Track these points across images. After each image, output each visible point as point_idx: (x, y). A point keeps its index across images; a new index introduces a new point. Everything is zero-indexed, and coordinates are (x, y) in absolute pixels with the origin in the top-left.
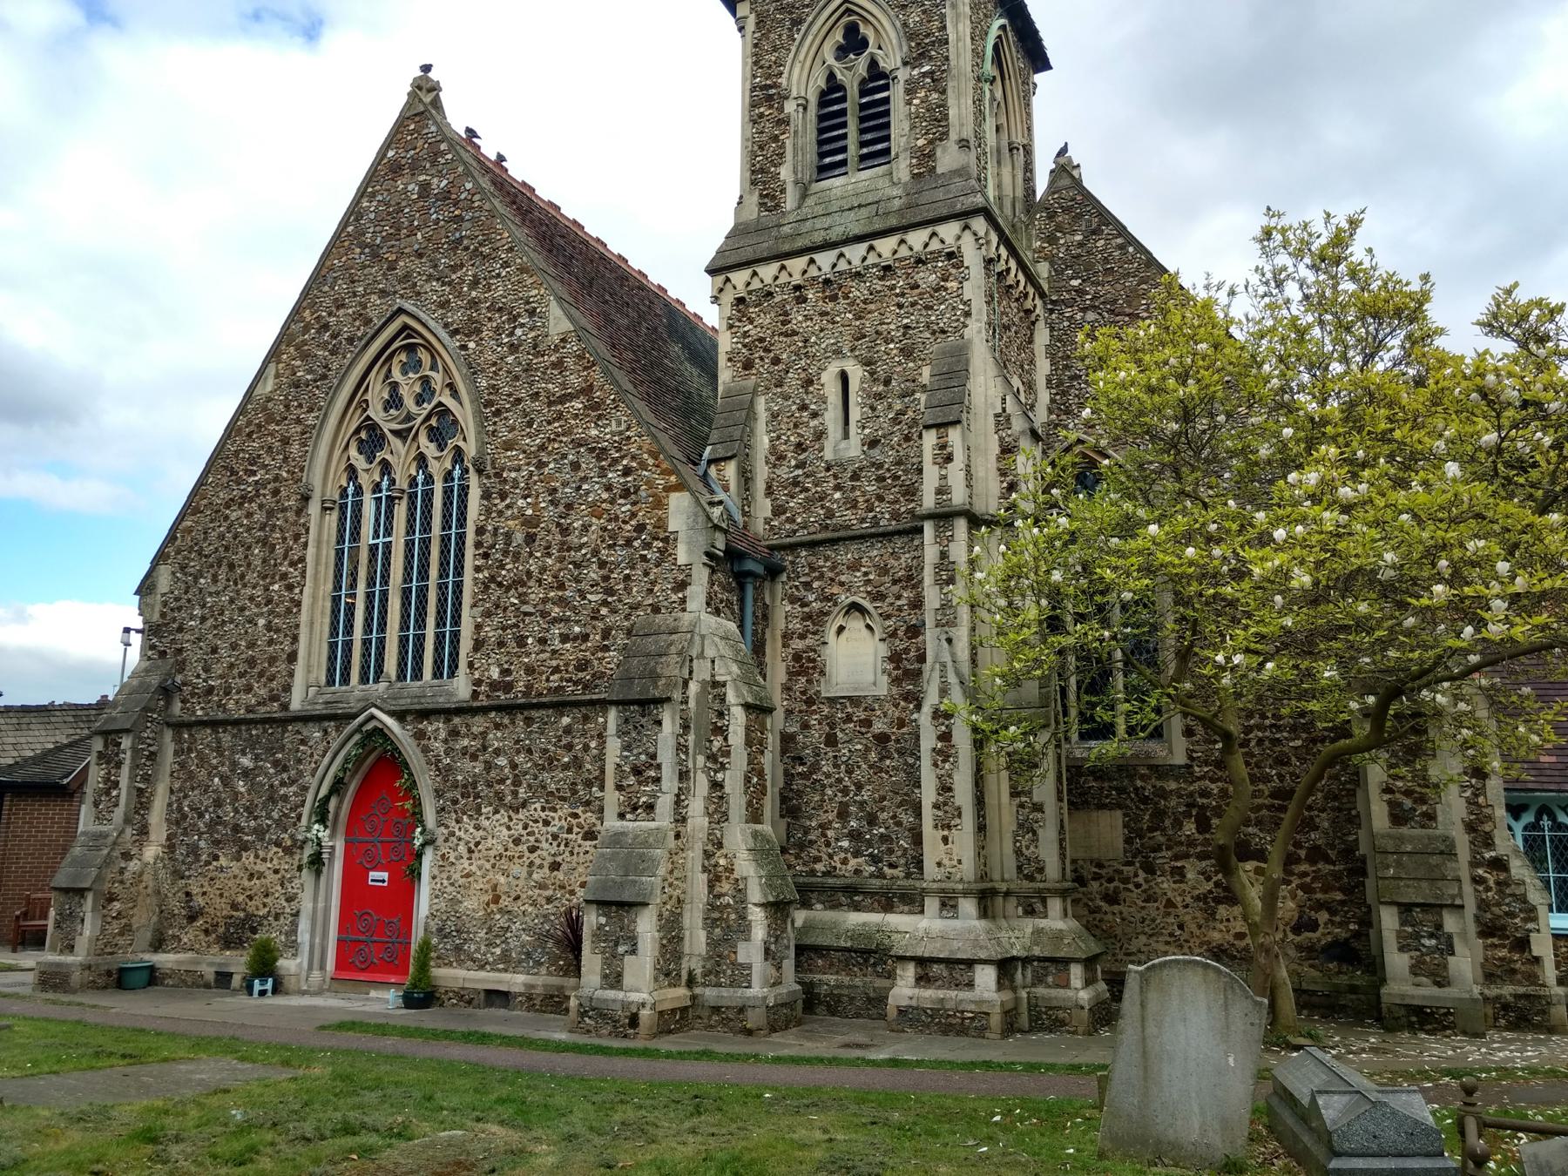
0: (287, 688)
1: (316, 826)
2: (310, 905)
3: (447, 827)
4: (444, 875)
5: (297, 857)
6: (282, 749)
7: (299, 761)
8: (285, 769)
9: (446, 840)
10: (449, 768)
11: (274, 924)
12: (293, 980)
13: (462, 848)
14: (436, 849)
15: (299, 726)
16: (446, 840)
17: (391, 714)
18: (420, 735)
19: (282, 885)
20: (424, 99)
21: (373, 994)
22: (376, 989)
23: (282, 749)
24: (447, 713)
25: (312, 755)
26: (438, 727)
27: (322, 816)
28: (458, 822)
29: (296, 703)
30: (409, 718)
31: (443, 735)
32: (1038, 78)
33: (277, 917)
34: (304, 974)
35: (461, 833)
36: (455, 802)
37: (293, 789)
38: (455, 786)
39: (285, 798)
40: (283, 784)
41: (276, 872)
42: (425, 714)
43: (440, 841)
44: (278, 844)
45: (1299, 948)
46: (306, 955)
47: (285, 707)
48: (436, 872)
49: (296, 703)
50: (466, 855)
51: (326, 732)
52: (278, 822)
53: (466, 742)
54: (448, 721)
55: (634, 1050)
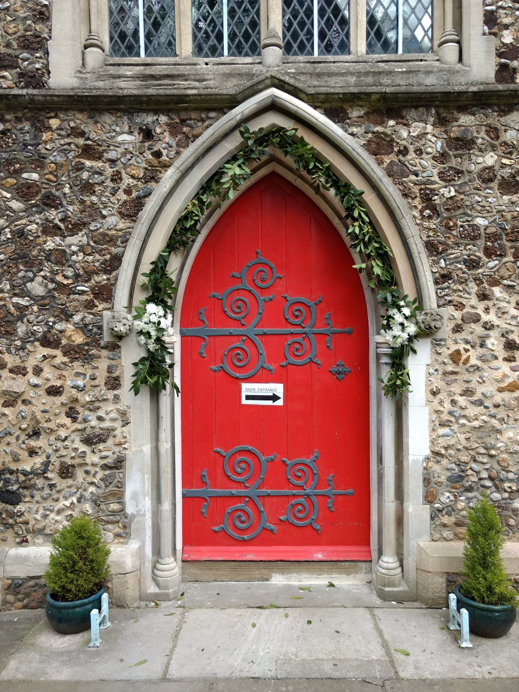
0: (36, 44)
1: (151, 307)
2: (147, 449)
3: (459, 306)
4: (457, 388)
5: (103, 364)
6: (39, 162)
7: (88, 188)
8: (50, 202)
9: (457, 329)
10: (454, 205)
11: (62, 484)
12: (131, 580)
13: (495, 342)
14: (437, 343)
15: (78, 120)
16: (457, 329)
17: (314, 100)
18: (380, 146)
19: (72, 414)
21: (278, 580)
22: (282, 572)
23: (39, 162)
24: (443, 104)
25: (116, 178)
26: (420, 132)
27: (158, 290)
28: (483, 297)
29: (64, 72)
30: (355, 113)
31: (436, 145)
33: (66, 472)
34: (148, 566)
35: (491, 317)
36: (473, 264)
37: (80, 238)
38: (472, 235)
39: (61, 257)
40: (50, 229)
41: (54, 391)
42: (393, 106)
43: (446, 330)
44: (47, 341)
45: (157, 32)
46: (149, 532)
47: (35, 79)
48: (438, 383)
49: (64, 72)
50: (501, 353)
51: (148, 134)
52: (44, 303)
53: (490, 159)
54: (442, 122)
55: (379, 471)
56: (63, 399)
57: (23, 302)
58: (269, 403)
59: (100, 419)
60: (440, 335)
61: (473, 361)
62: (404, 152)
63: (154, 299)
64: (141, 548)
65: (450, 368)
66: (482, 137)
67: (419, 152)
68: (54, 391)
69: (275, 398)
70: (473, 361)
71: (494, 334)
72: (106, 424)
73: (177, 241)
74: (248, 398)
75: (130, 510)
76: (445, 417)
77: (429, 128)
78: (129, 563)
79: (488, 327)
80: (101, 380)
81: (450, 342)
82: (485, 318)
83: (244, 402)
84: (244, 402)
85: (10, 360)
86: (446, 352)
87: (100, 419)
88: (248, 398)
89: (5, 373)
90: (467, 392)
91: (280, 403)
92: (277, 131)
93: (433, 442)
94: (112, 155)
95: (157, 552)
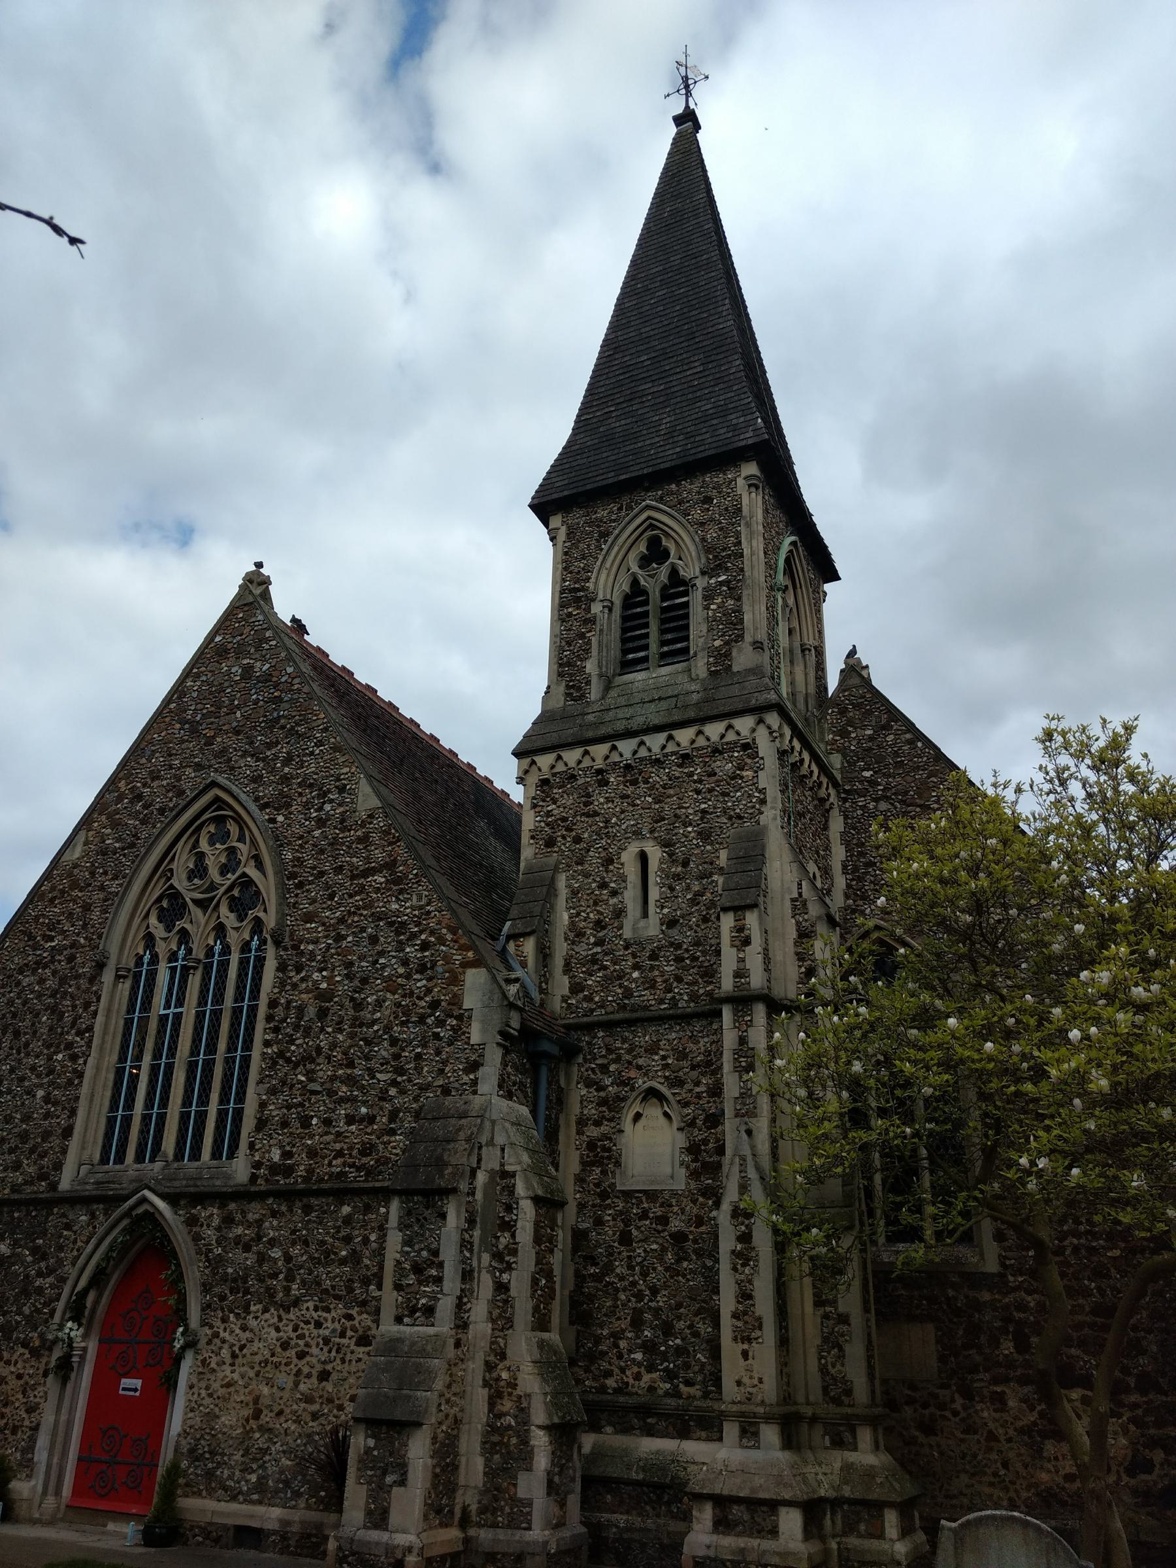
2: (52, 1419)
3: (211, 1327)
6: (43, 1234)
9: (209, 1343)
12: (25, 1505)
18: (192, 1221)
20: (839, 579)
24: (221, 1198)
26: (212, 1214)
28: (224, 1320)
32: (828, 587)
35: (226, 1335)
36: (223, 1298)
50: (228, 1360)
53: (239, 1231)
54: (222, 1206)
56: (22, 1382)
57: (18, 1318)
58: (132, 1393)
59: (35, 1396)
60: (200, 1346)
61: (213, 1365)
62: (202, 1226)
63: (76, 1318)
64: (35, 1487)
65: (200, 1370)
66: (238, 1217)
67: (208, 1226)
68: (19, 1377)
69: (135, 1390)
70: (213, 1365)
71: (226, 1346)
72: (37, 1400)
73: (98, 1279)
74: (124, 1389)
75: (35, 1459)
76: (193, 1404)
77: (215, 1211)
78: (26, 1494)
79: (224, 1341)
80: (41, 1371)
81: (204, 1351)
82: (222, 1334)
83: (121, 1392)
84: (121, 1392)
85: (6, 1355)
86: (200, 1358)
87: (35, 1396)
88: (124, 1389)
89: (2, 1364)
90: (207, 1388)
91: (138, 1394)
92: (146, 1212)
93: (184, 1421)
94: (75, 1228)
95: (45, 1493)
